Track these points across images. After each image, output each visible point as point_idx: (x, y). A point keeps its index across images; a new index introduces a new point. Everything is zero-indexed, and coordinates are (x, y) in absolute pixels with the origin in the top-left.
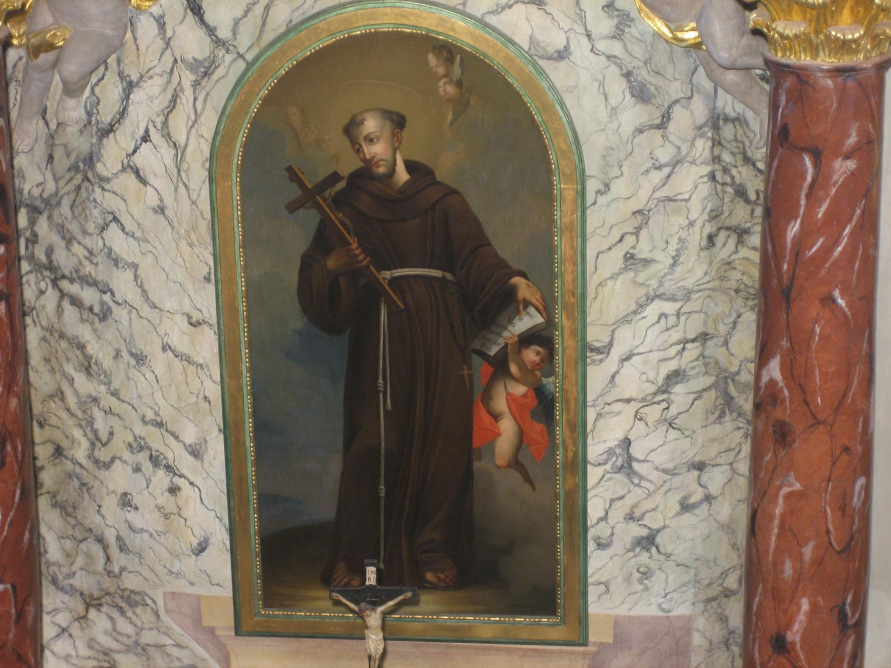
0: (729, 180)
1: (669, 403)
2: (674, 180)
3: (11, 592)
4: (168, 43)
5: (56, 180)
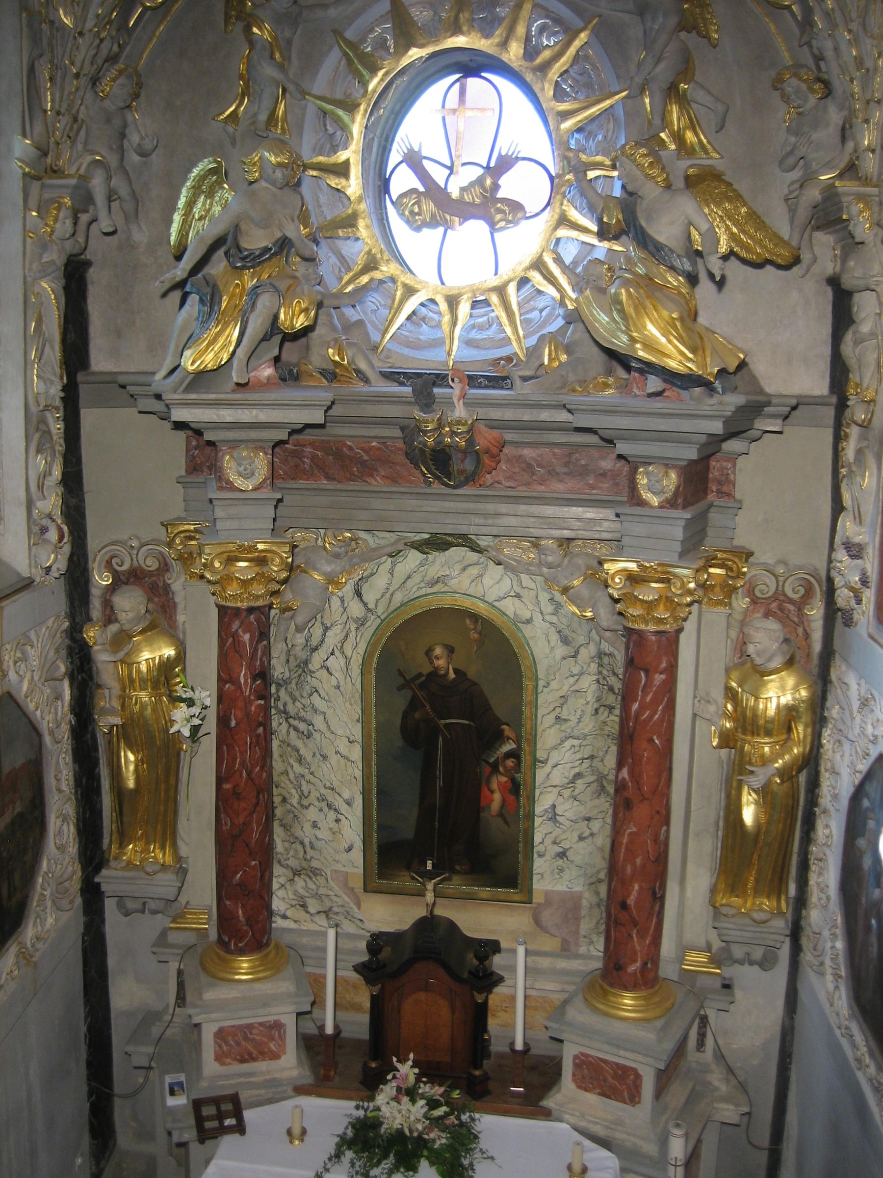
1: (575, 788)
5: (290, 671)
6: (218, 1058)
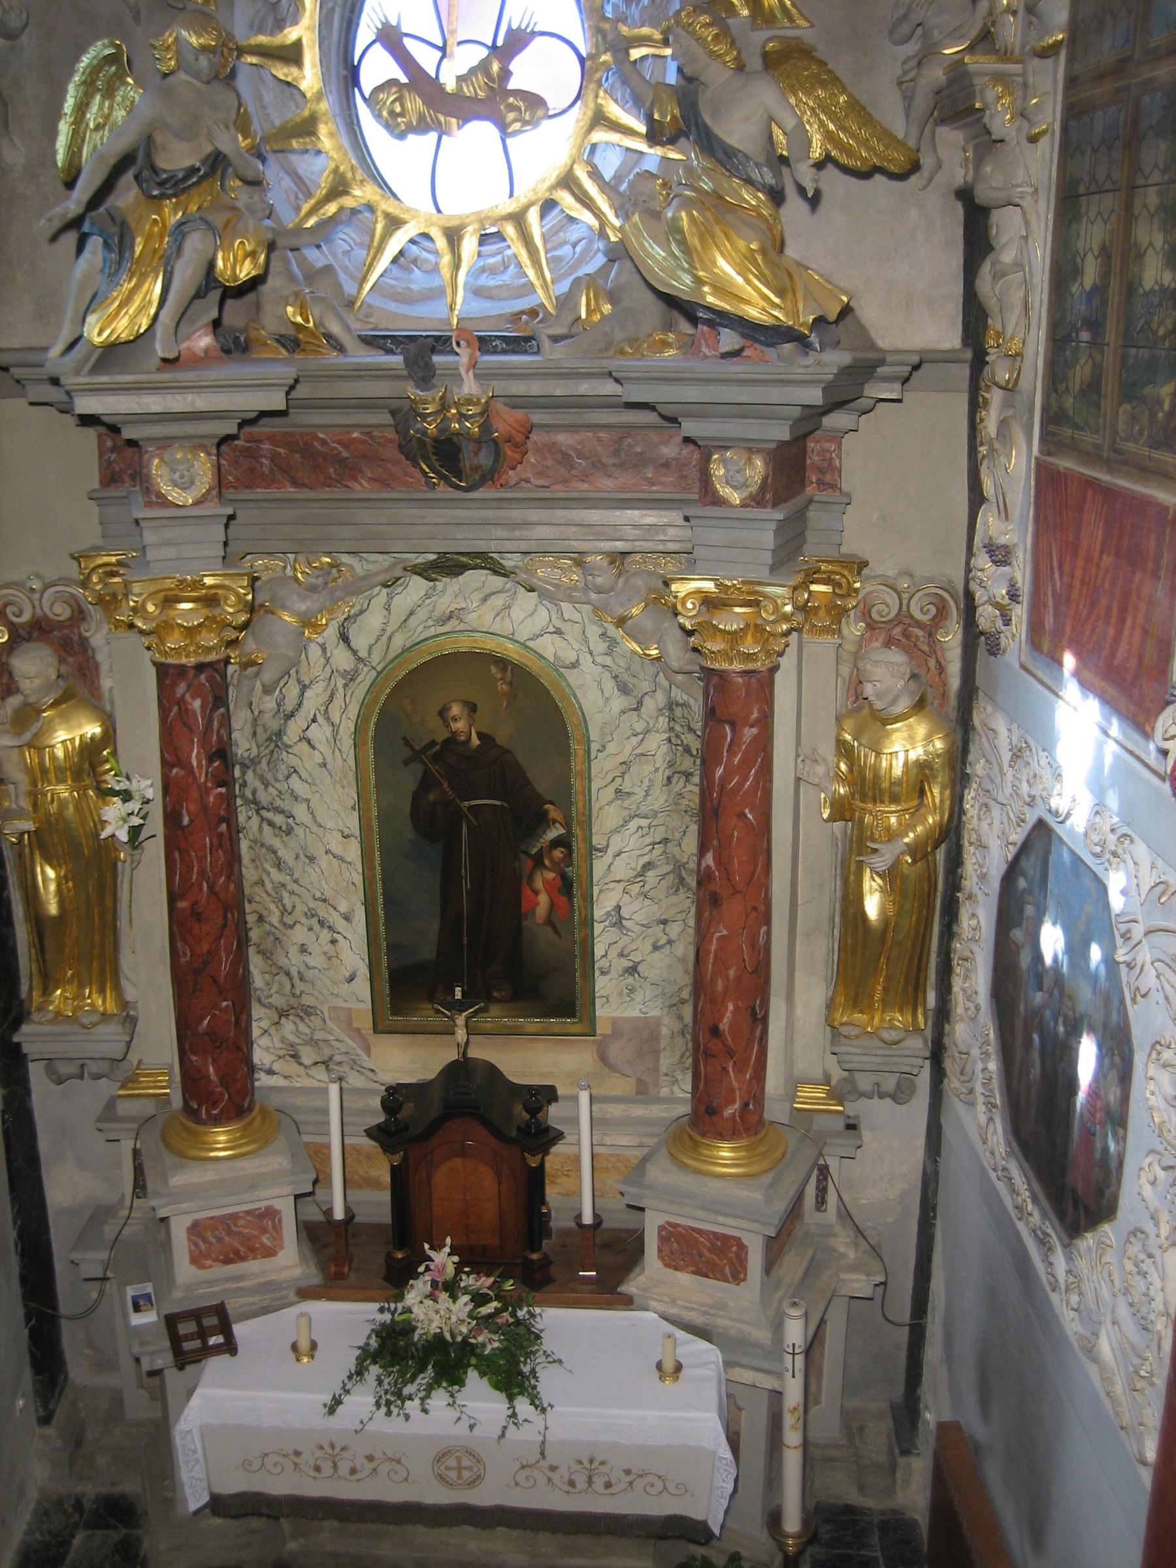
1: (645, 882)
5: (258, 747)
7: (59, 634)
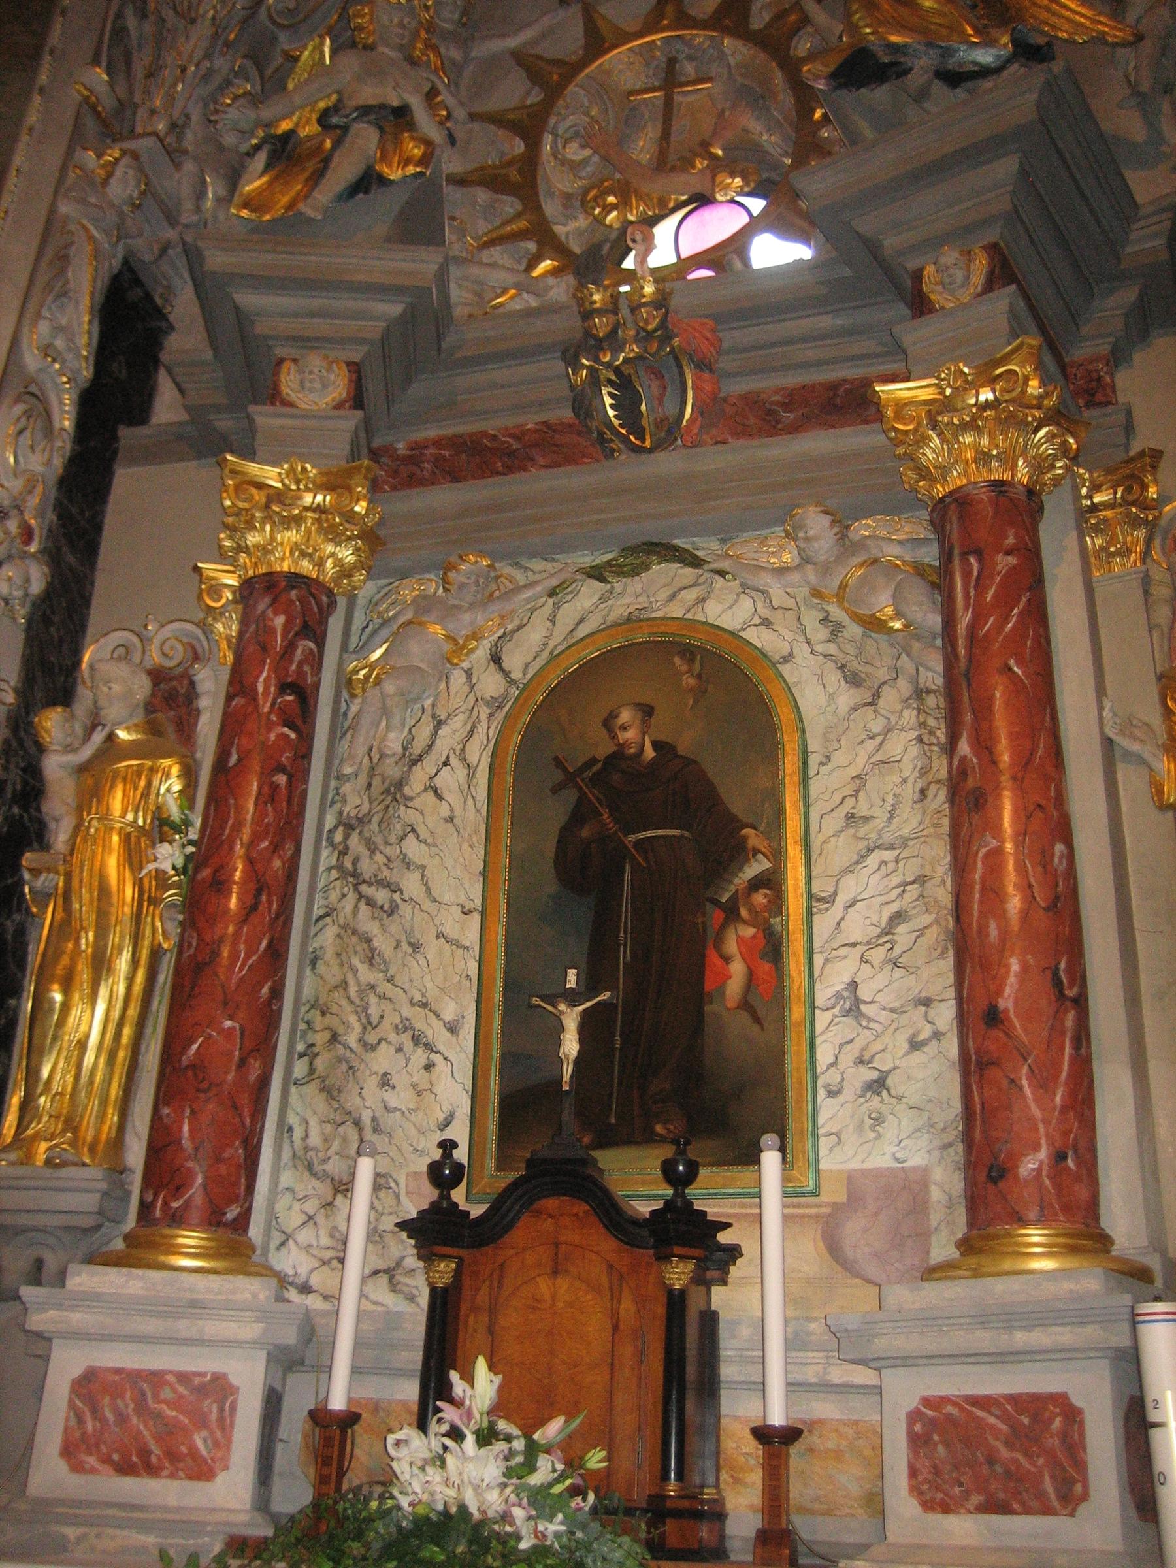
0: (935, 741)
1: (893, 943)
2: (886, 746)
3: (238, 1032)
4: (472, 688)
5: (371, 802)
6: (69, 1451)
7: (167, 687)
